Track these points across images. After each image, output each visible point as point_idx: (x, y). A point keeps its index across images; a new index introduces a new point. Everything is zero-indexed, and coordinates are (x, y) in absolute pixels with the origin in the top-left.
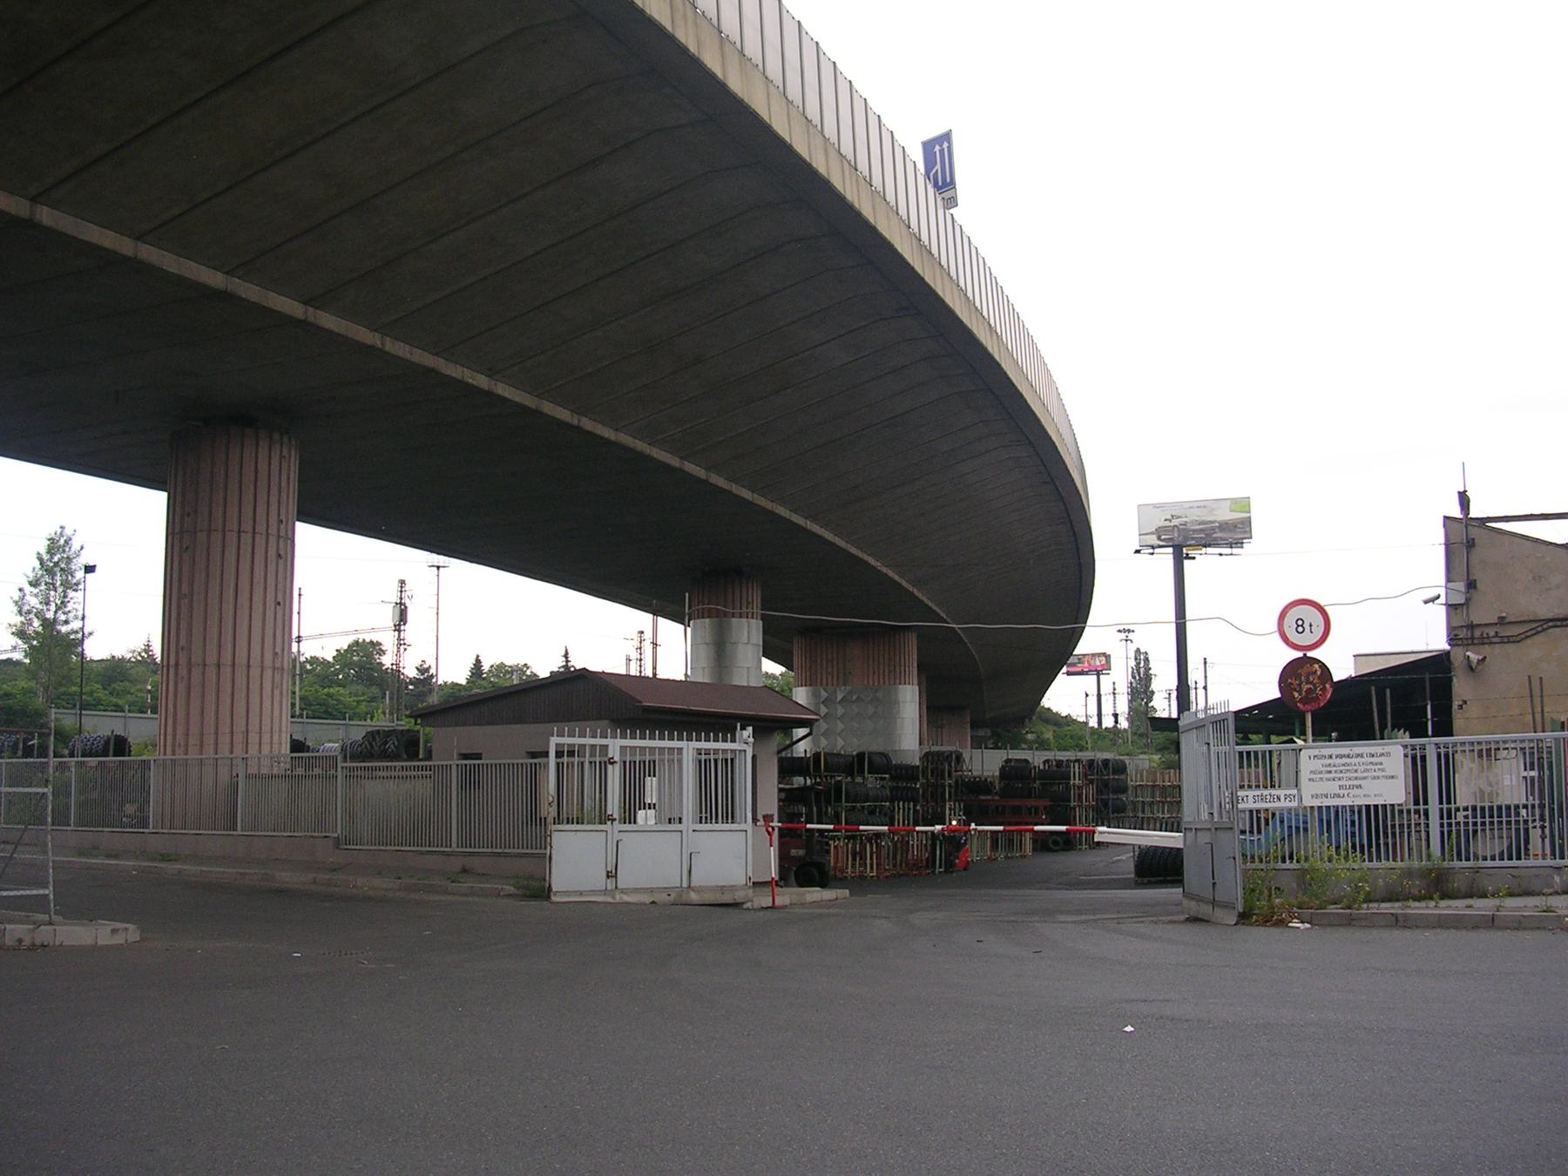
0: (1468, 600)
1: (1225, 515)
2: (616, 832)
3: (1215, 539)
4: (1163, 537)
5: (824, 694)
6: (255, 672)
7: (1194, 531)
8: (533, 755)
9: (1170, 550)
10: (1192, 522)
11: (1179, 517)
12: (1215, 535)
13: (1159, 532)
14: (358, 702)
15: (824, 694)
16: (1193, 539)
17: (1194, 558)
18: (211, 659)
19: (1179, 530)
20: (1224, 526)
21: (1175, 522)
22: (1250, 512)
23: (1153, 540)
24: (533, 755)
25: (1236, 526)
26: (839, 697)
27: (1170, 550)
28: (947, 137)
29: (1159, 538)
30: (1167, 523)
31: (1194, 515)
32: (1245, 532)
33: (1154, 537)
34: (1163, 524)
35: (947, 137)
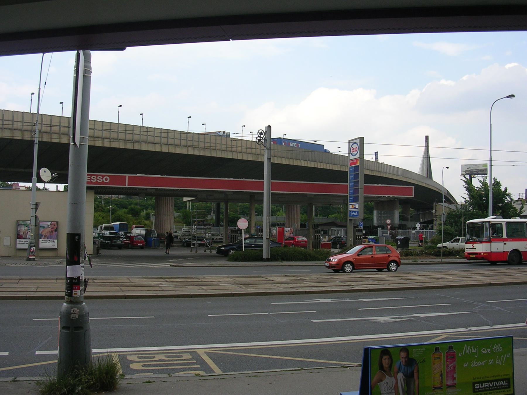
0: (435, 212)
1: (482, 168)
2: (485, 385)
3: (479, 173)
4: (467, 173)
5: (380, 212)
6: (294, 219)
7: (474, 171)
8: (329, 229)
9: (469, 176)
10: (474, 169)
11: (471, 168)
12: (479, 173)
13: (466, 171)
14: (275, 207)
15: (380, 212)
16: (474, 173)
17: (475, 177)
18: (292, 218)
19: (470, 171)
20: (481, 170)
21: (470, 169)
22: (487, 167)
23: (464, 173)
24: (329, 229)
25: (484, 171)
26: (383, 213)
27: (469, 176)
28: (377, 152)
29: (466, 173)
30: (468, 169)
31: (474, 168)
32: (486, 172)
33: (465, 173)
34: (467, 169)
35: (377, 152)
